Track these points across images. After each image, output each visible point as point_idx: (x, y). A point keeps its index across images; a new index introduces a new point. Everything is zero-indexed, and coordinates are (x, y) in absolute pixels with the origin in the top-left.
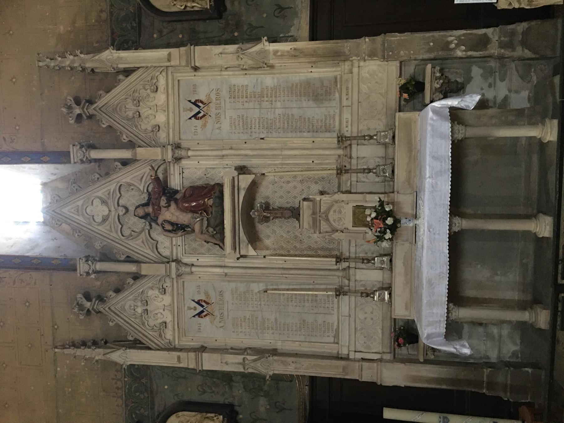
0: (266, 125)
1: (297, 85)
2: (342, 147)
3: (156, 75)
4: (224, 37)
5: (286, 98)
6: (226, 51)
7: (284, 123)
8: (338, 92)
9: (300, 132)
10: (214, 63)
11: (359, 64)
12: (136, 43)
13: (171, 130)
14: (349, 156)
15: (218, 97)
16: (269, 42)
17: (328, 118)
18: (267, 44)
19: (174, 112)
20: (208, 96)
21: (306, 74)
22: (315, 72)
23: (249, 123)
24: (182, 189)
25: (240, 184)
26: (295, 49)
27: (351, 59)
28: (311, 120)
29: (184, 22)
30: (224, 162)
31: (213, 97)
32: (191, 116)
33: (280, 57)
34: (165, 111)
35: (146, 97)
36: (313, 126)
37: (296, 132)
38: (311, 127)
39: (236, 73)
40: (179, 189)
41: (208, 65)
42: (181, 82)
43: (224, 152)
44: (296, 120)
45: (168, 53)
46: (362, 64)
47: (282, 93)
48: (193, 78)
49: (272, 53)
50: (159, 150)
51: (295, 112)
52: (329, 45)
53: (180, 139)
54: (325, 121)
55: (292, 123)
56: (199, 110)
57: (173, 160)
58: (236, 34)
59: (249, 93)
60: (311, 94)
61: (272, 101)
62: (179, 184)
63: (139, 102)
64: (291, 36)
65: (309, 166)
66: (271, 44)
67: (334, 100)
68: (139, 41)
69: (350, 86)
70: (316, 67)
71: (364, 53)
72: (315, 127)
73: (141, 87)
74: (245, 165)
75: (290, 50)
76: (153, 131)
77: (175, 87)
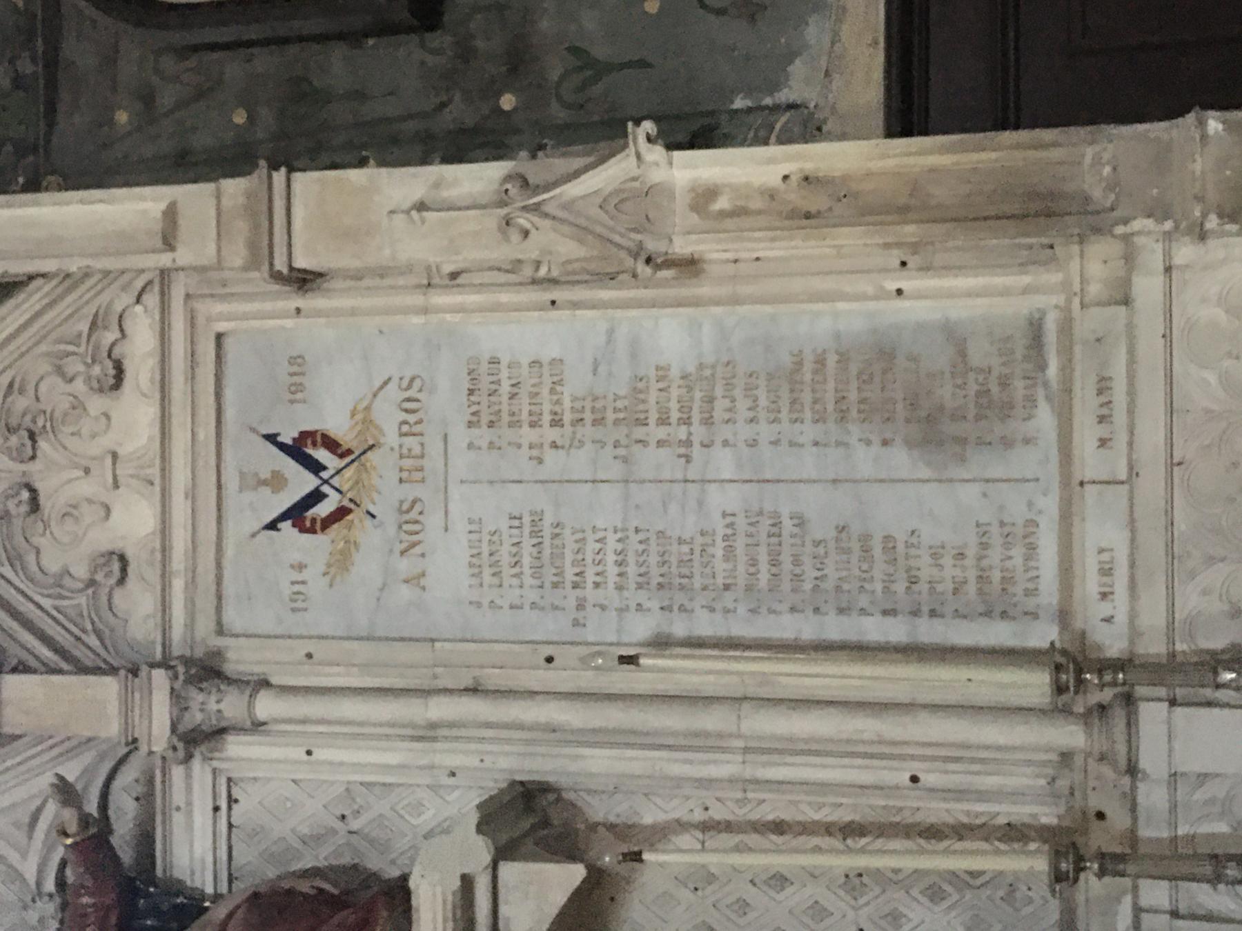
0: (655, 572)
1: (821, 362)
2: (1079, 709)
3: (118, 308)
4: (448, 119)
5: (765, 431)
6: (447, 194)
7: (754, 562)
8: (1048, 398)
9: (841, 611)
10: (387, 252)
11: (1167, 255)
12: (35, 149)
13: (178, 584)
14: (1123, 763)
15: (412, 418)
16: (671, 146)
17: (996, 539)
18: (656, 153)
19: (192, 494)
20: (364, 417)
21: (872, 305)
22: (919, 296)
23: (569, 557)
24: (224, 888)
25: (503, 910)
26: (806, 179)
27: (1120, 230)
28: (901, 547)
29: (255, 50)
30: (438, 759)
31: (388, 417)
32: (274, 514)
33: (729, 223)
34: (152, 484)
35: (66, 414)
36: (913, 581)
37: (817, 610)
38: (900, 587)
39: (505, 297)
40: (209, 890)
41: (355, 264)
42: (228, 343)
43: (439, 709)
44: (817, 544)
45: (163, 206)
46: (1185, 252)
47: (742, 405)
48: (289, 323)
49: (682, 201)
50: (109, 687)
51: (812, 501)
52: (993, 155)
53: (220, 631)
54: (980, 558)
55: (797, 562)
56: (316, 482)
57: (175, 749)
58: (507, 102)
59: (567, 403)
60: (900, 406)
61: (688, 443)
62: (210, 859)
63: (32, 436)
64: (792, 106)
65: (891, 803)
66: (677, 155)
67: (1027, 441)
68: (48, 141)
69: (1118, 371)
70: (926, 269)
71: (1199, 199)
72: (923, 587)
73: (45, 367)
74: (551, 779)
75: (782, 186)
76: (92, 583)
77: (199, 371)
